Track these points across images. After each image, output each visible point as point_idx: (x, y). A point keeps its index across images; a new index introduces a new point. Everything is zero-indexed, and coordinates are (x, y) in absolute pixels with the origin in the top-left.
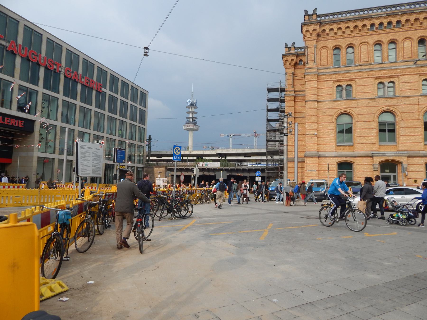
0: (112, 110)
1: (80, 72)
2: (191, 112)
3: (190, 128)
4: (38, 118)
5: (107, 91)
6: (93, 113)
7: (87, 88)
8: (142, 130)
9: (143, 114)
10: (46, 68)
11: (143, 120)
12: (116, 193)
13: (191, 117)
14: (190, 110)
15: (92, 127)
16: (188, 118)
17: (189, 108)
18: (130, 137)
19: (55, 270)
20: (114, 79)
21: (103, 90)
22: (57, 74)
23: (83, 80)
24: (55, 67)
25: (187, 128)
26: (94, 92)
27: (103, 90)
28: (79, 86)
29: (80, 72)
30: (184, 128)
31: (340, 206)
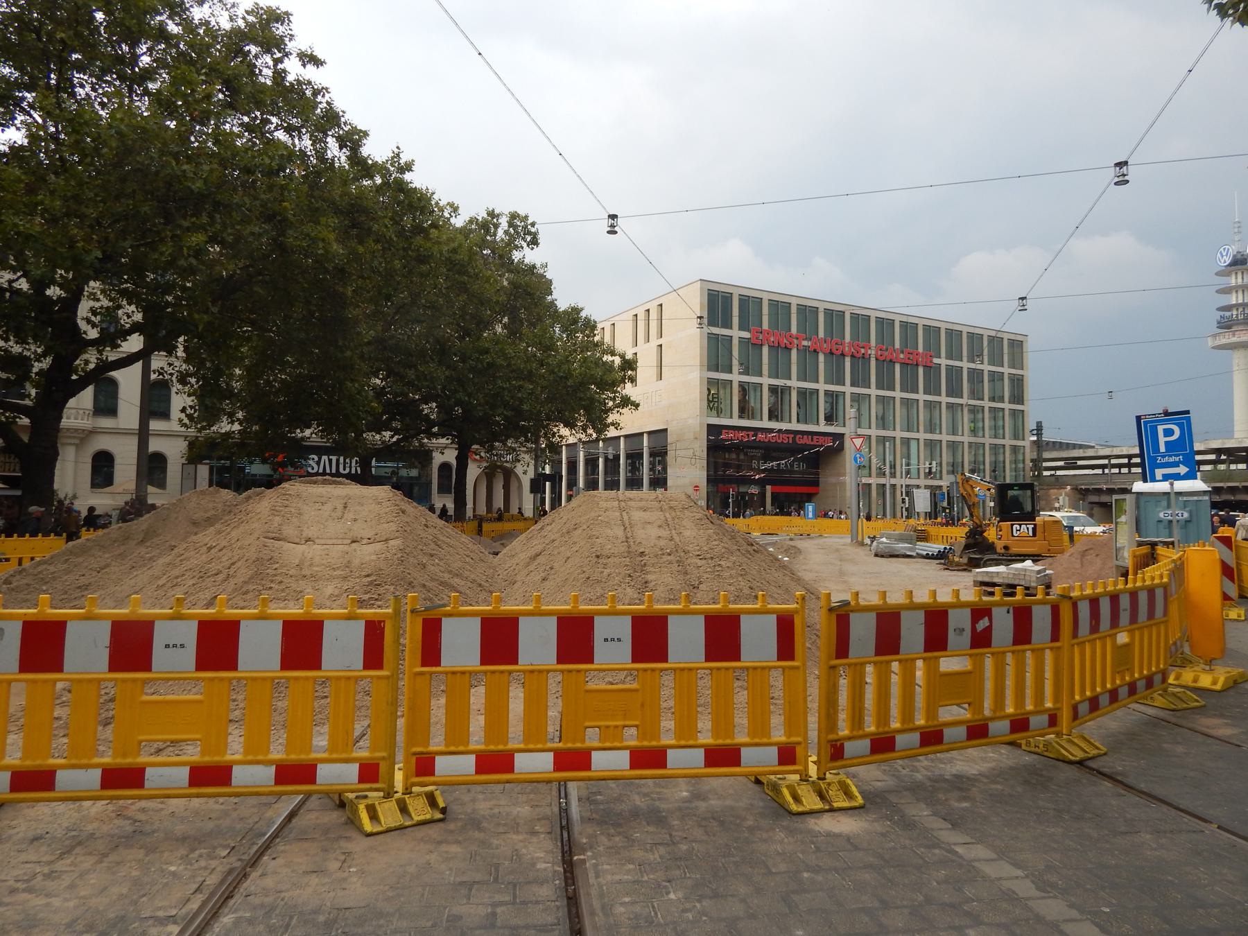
0: (954, 391)
1: (897, 345)
2: (1236, 289)
3: (1234, 339)
4: (848, 430)
5: (943, 361)
6: (921, 404)
7: (910, 366)
8: (1018, 416)
9: (1018, 384)
10: (853, 356)
11: (1018, 397)
12: (1165, 587)
13: (1237, 306)
14: (1233, 281)
15: (921, 428)
16: (1228, 308)
17: (1228, 274)
18: (578, 872)
19: (851, 816)
20: (954, 335)
21: (936, 361)
22: (866, 359)
23: (902, 356)
24: (863, 351)
25: (1224, 341)
26: (921, 370)
27: (936, 361)
28: (897, 367)
29: (897, 345)
30: (1210, 342)
31: (26, 439)
